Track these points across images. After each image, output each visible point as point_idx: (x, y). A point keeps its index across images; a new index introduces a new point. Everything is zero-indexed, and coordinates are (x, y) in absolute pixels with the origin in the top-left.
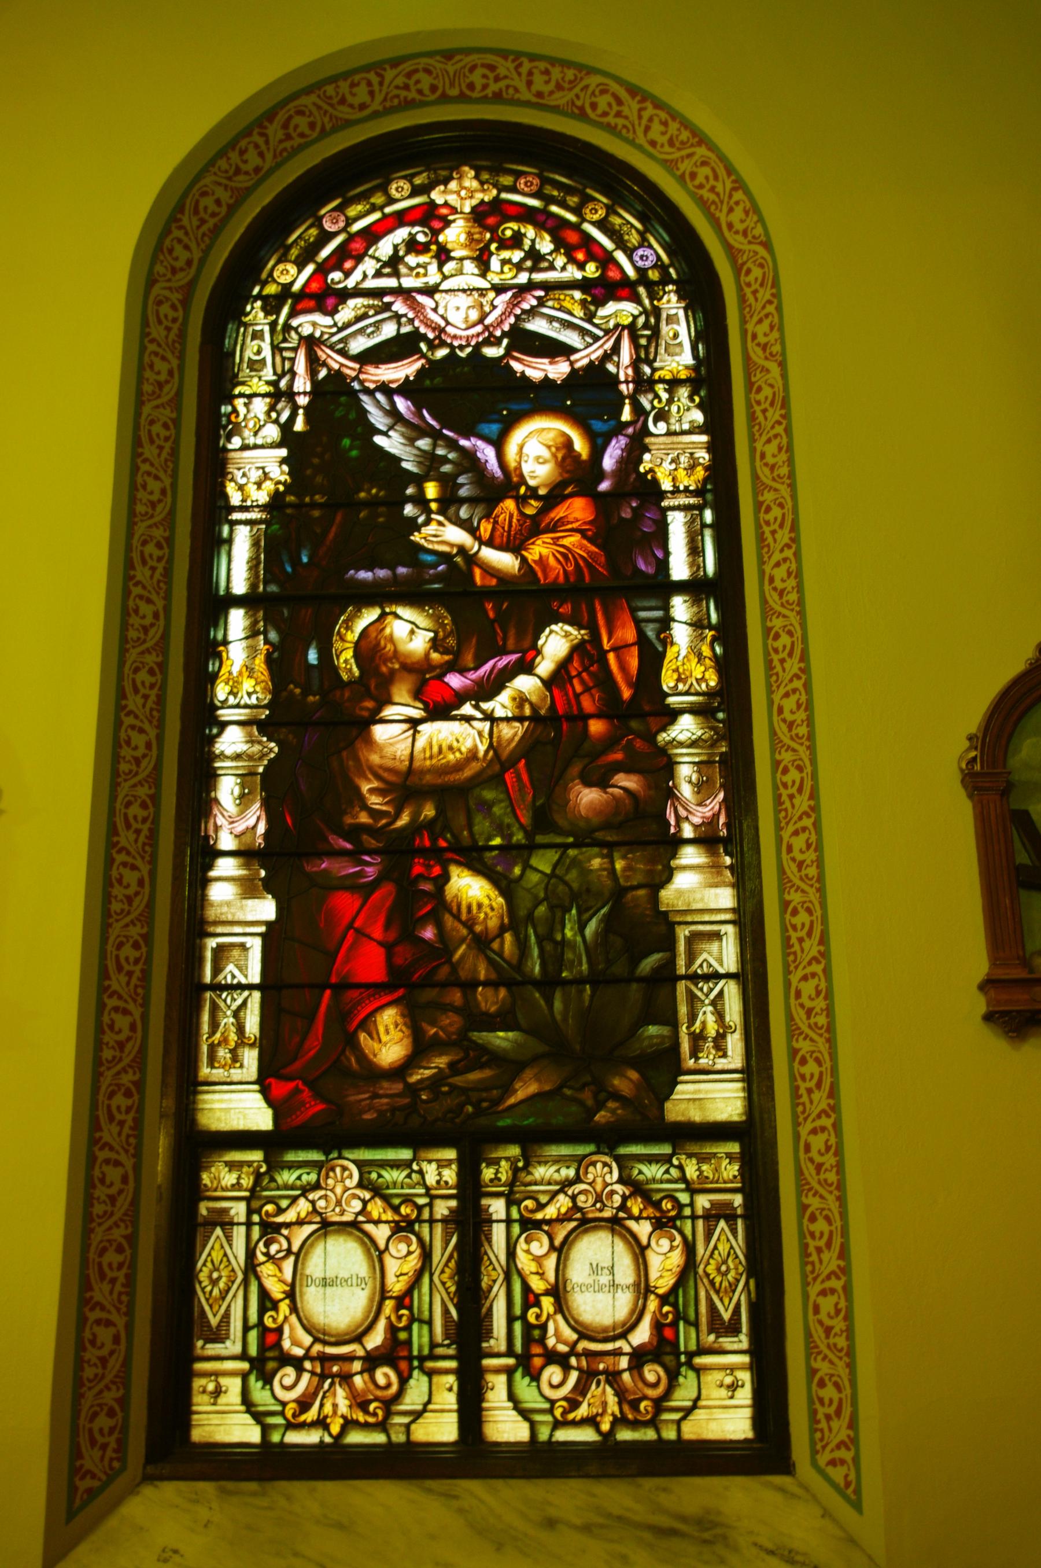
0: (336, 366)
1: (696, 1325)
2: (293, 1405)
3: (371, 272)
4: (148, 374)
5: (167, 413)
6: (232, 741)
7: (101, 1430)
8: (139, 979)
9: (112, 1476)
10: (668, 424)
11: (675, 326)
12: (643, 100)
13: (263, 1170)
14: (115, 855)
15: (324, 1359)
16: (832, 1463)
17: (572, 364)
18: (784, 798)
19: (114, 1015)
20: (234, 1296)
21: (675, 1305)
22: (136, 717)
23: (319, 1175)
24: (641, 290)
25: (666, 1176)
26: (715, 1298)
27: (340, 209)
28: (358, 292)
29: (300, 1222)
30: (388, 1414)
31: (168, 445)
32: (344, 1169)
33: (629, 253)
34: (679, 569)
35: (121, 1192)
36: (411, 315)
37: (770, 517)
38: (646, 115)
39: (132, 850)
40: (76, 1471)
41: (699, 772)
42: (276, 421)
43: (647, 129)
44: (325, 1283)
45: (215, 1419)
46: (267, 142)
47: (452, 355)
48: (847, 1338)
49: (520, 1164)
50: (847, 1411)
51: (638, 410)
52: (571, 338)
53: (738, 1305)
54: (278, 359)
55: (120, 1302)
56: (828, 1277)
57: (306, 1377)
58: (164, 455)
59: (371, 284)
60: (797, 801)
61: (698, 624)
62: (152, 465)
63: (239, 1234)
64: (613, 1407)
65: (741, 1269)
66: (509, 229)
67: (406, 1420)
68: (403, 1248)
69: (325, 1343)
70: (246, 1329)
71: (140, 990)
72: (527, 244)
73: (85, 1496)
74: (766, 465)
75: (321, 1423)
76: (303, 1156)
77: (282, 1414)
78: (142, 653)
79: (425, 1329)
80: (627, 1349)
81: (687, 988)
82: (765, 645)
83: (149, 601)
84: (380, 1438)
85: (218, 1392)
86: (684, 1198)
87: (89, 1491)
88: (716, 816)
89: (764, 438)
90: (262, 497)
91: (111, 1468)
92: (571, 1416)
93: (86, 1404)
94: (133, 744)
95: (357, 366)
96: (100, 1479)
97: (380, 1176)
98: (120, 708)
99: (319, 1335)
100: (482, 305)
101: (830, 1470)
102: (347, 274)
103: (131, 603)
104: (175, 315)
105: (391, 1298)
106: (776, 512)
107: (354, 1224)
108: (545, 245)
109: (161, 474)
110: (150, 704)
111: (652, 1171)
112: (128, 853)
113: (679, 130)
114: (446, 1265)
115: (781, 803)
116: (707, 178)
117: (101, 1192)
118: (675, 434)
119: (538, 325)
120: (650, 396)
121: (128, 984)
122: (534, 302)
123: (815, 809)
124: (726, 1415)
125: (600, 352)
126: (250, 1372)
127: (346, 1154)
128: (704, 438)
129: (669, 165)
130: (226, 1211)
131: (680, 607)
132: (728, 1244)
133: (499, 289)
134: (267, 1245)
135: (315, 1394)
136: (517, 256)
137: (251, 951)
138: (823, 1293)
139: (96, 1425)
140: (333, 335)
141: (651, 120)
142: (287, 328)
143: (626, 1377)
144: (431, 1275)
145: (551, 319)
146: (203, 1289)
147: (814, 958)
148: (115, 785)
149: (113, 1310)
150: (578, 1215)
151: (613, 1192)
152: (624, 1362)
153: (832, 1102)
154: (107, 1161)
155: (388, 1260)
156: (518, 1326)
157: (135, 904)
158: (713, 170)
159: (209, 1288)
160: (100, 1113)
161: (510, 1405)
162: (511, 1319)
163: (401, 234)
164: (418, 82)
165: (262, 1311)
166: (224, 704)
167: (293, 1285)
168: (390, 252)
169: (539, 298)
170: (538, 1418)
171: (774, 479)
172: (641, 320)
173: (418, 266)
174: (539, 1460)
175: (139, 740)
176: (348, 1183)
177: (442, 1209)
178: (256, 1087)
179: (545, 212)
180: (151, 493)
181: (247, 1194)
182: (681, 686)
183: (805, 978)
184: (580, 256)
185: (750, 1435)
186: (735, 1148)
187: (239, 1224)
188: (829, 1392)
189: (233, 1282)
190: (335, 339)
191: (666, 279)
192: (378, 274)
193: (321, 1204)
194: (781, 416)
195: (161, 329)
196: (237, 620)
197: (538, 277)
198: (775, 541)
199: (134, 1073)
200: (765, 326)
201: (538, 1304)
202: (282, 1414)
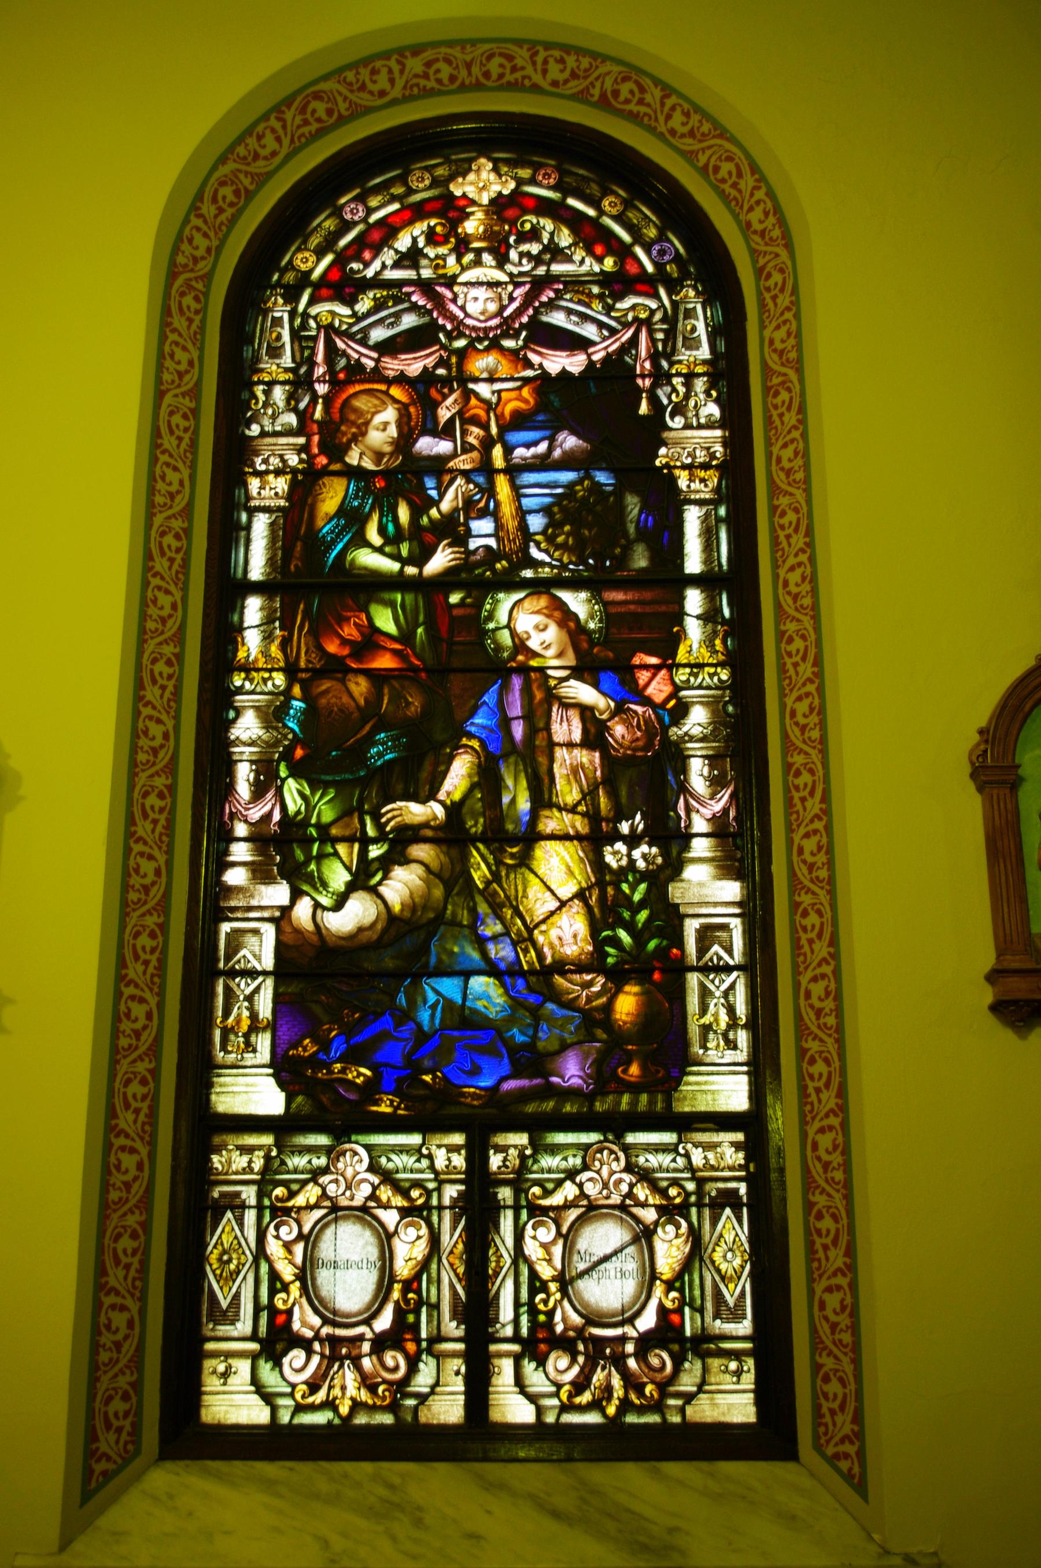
1: (701, 1310)
2: (304, 1387)
3: (389, 263)
4: (168, 363)
6: (247, 727)
7: (116, 1414)
8: (129, 1434)
9: (127, 1458)
10: (686, 418)
13: (528, 1152)
14: (132, 845)
15: (334, 1341)
17: (589, 356)
18: (789, 666)
20: (245, 1278)
21: (681, 1290)
22: (154, 708)
25: (673, 1165)
27: (361, 199)
28: (376, 282)
29: (310, 1208)
31: (187, 437)
32: (356, 1153)
34: (693, 563)
35: (135, 1179)
37: (785, 521)
39: (139, 982)
40: (91, 1454)
41: (710, 765)
42: (295, 410)
43: (669, 117)
46: (284, 127)
48: (845, 1172)
49: (274, 1153)
51: (654, 401)
52: (590, 331)
54: (296, 347)
55: (134, 1287)
56: (835, 1274)
57: (316, 1359)
58: (183, 445)
59: (391, 275)
60: (809, 804)
62: (180, 335)
63: (250, 1216)
64: (619, 1392)
65: (746, 1257)
66: (530, 220)
67: (680, 1402)
68: (412, 1232)
69: (335, 1324)
71: (164, 838)
73: (101, 1479)
75: (330, 1404)
78: (152, 776)
80: (369, 1335)
81: (702, 985)
82: (806, 1223)
83: (159, 721)
84: (654, 1418)
85: (225, 1375)
86: (691, 1186)
87: (105, 1473)
88: (725, 811)
89: (780, 443)
91: (126, 1451)
93: (102, 1386)
94: (142, 871)
95: (375, 355)
96: (115, 1462)
97: (389, 1160)
98: (139, 698)
100: (500, 299)
102: (367, 265)
103: (150, 594)
105: (398, 1282)
106: (791, 516)
107: (364, 1209)
108: (565, 239)
110: (159, 829)
111: (654, 1160)
112: (145, 843)
113: (700, 121)
115: (786, 671)
116: (730, 173)
117: (107, 1339)
120: (669, 389)
121: (144, 973)
122: (552, 294)
123: (835, 956)
124: (731, 1401)
127: (354, 1138)
128: (718, 433)
129: (689, 156)
130: (238, 1194)
131: (694, 600)
132: (731, 1233)
134: (277, 1228)
135: (325, 1376)
136: (535, 248)
138: (829, 1290)
139: (111, 1410)
140: (351, 325)
142: (305, 315)
143: (632, 1363)
144: (440, 1260)
145: (569, 312)
146: (214, 1271)
148: (142, 642)
149: (156, 848)
154: (123, 1149)
155: (396, 1242)
157: (143, 1038)
158: (737, 166)
159: (218, 1272)
160: (106, 1257)
161: (517, 1389)
162: (517, 1304)
163: (419, 229)
165: (273, 1292)
166: (240, 691)
167: (303, 1269)
169: (557, 291)
171: (789, 484)
172: (658, 316)
173: (437, 257)
175: (156, 730)
176: (358, 1168)
177: (451, 1192)
178: (271, 1071)
179: (562, 204)
180: (170, 484)
181: (258, 1177)
182: (692, 679)
183: (807, 835)
184: (599, 250)
185: (752, 1419)
186: (740, 1137)
187: (250, 1207)
188: (834, 1387)
190: (355, 329)
191: (684, 275)
192: (396, 265)
193: (331, 1190)
194: (806, 543)
195: (183, 321)
197: (557, 268)
198: (790, 545)
199: (141, 1214)
200: (782, 333)
202: (292, 1395)
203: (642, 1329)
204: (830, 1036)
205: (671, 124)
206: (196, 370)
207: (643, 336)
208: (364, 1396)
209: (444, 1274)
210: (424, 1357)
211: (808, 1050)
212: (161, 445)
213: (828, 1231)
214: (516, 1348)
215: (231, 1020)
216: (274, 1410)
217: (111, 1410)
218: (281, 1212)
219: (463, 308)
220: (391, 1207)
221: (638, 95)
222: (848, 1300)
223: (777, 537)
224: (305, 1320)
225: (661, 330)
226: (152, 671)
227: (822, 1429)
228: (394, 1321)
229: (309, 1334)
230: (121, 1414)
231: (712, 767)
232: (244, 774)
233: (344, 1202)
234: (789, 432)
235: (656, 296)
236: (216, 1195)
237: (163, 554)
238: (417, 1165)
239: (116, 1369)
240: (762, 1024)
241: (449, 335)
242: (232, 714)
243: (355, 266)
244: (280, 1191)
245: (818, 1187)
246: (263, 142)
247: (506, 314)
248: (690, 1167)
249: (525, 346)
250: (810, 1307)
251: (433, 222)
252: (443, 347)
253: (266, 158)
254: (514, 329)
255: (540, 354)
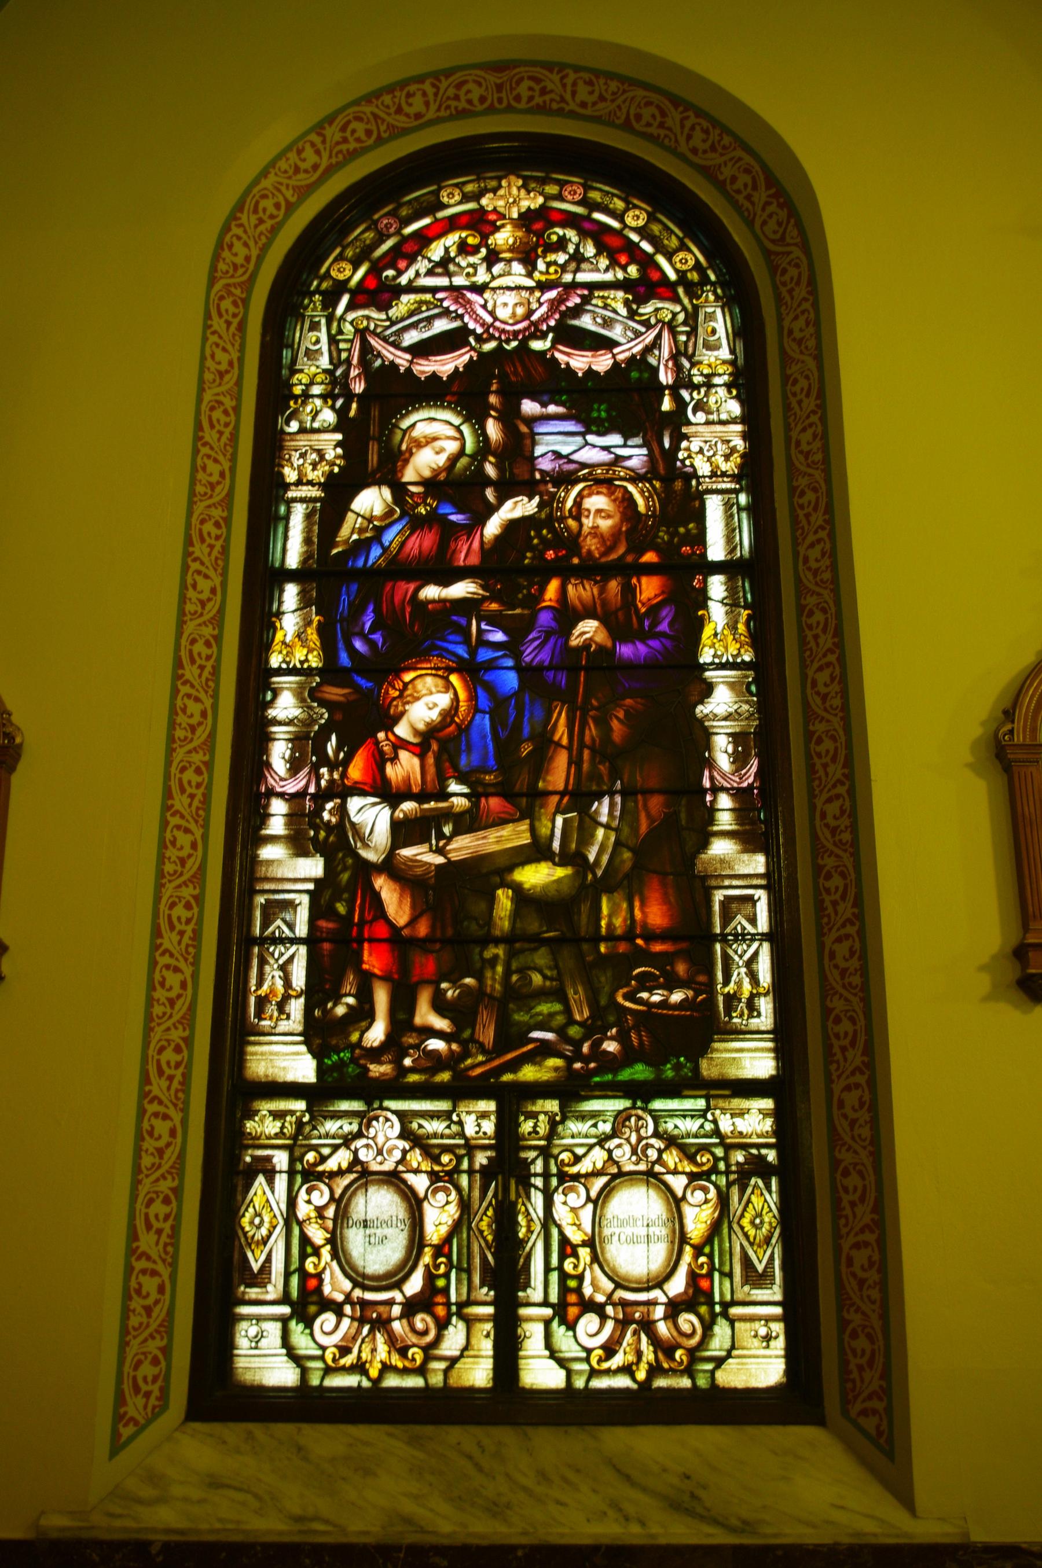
0: (391, 357)
1: (730, 1275)
3: (423, 271)
5: (217, 513)
6: (286, 706)
8: (168, 1236)
11: (712, 324)
12: (686, 110)
14: (169, 818)
16: (864, 1413)
17: (614, 356)
18: (818, 767)
19: (165, 972)
22: (192, 686)
23: (360, 1125)
24: (681, 291)
25: (702, 1131)
26: (751, 1253)
30: (428, 1358)
32: (387, 1120)
33: (669, 256)
34: (716, 552)
36: (460, 311)
38: (688, 124)
42: (333, 408)
44: (365, 1224)
45: (255, 1363)
47: (499, 349)
49: (558, 1118)
50: (879, 1361)
52: (616, 333)
53: (772, 1258)
57: (346, 1322)
58: (224, 439)
60: (841, 908)
61: (732, 603)
62: (212, 448)
69: (365, 1288)
70: (287, 1275)
71: (191, 950)
72: (571, 249)
74: (801, 452)
75: (360, 1368)
76: (345, 1106)
77: (322, 1358)
79: (464, 1276)
80: (663, 1299)
82: (824, 1028)
83: (197, 700)
85: (259, 1337)
86: (719, 1152)
90: (317, 475)
92: (605, 1365)
95: (408, 357)
99: (360, 1279)
100: (529, 303)
101: (862, 1420)
102: (400, 273)
104: (228, 419)
106: (810, 496)
108: (590, 250)
109: (221, 458)
110: (196, 803)
113: (720, 135)
114: (485, 1213)
116: (746, 185)
117: (149, 1144)
118: (713, 423)
119: (586, 322)
121: (180, 943)
124: (759, 1364)
125: (640, 347)
126: (291, 1317)
127: (387, 1103)
128: (739, 428)
131: (717, 586)
132: (763, 1201)
133: (543, 287)
134: (309, 1192)
135: (354, 1339)
136: (562, 258)
137: (299, 908)
139: (139, 1375)
140: (387, 328)
141: (693, 128)
147: (848, 920)
149: (159, 1261)
150: (359, 1168)
151: (648, 1146)
152: (659, 1312)
153: (876, 1217)
154: (156, 1115)
156: (554, 1277)
158: (754, 179)
160: (150, 1067)
161: (547, 1353)
162: (548, 1270)
163: (452, 239)
164: (468, 92)
167: (333, 1233)
168: (442, 253)
169: (582, 297)
170: (577, 1366)
171: (808, 466)
172: (681, 317)
173: (470, 265)
174: (574, 1408)
175: (194, 708)
177: (481, 1159)
183: (839, 940)
184: (623, 260)
186: (768, 1104)
187: (281, 1172)
189: (274, 1227)
192: (430, 273)
193: (363, 1155)
196: (291, 593)
200: (801, 322)
201: (575, 1255)
203: (671, 1294)
204: (855, 995)
205: (692, 143)
206: (236, 370)
207: (666, 334)
208: (396, 1361)
209: (473, 1239)
210: (454, 1319)
211: (841, 1161)
212: (211, 326)
213: (846, 1034)
214: (548, 1312)
215: (265, 987)
216: (304, 1372)
217: (139, 1375)
218: (312, 1175)
219: (492, 313)
220: (421, 1172)
221: (659, 119)
222: (867, 1097)
223: (814, 765)
224: (336, 1285)
225: (682, 333)
226: (180, 780)
227: (849, 1385)
228: (424, 1285)
229: (340, 1297)
230: (150, 1379)
231: (736, 744)
232: (279, 753)
233: (374, 1167)
234: (825, 655)
235: (677, 300)
236: (248, 1159)
237: (193, 661)
238: (447, 1131)
239: (158, 1174)
240: (785, 989)
241: (479, 339)
242: (269, 696)
243: (390, 273)
244: (311, 1157)
245: (844, 1144)
246: (303, 156)
247: (535, 317)
248: (717, 1132)
249: (553, 347)
250: (812, 819)
251: (464, 235)
252: (473, 349)
253: (306, 171)
254: (542, 331)
255: (568, 354)
